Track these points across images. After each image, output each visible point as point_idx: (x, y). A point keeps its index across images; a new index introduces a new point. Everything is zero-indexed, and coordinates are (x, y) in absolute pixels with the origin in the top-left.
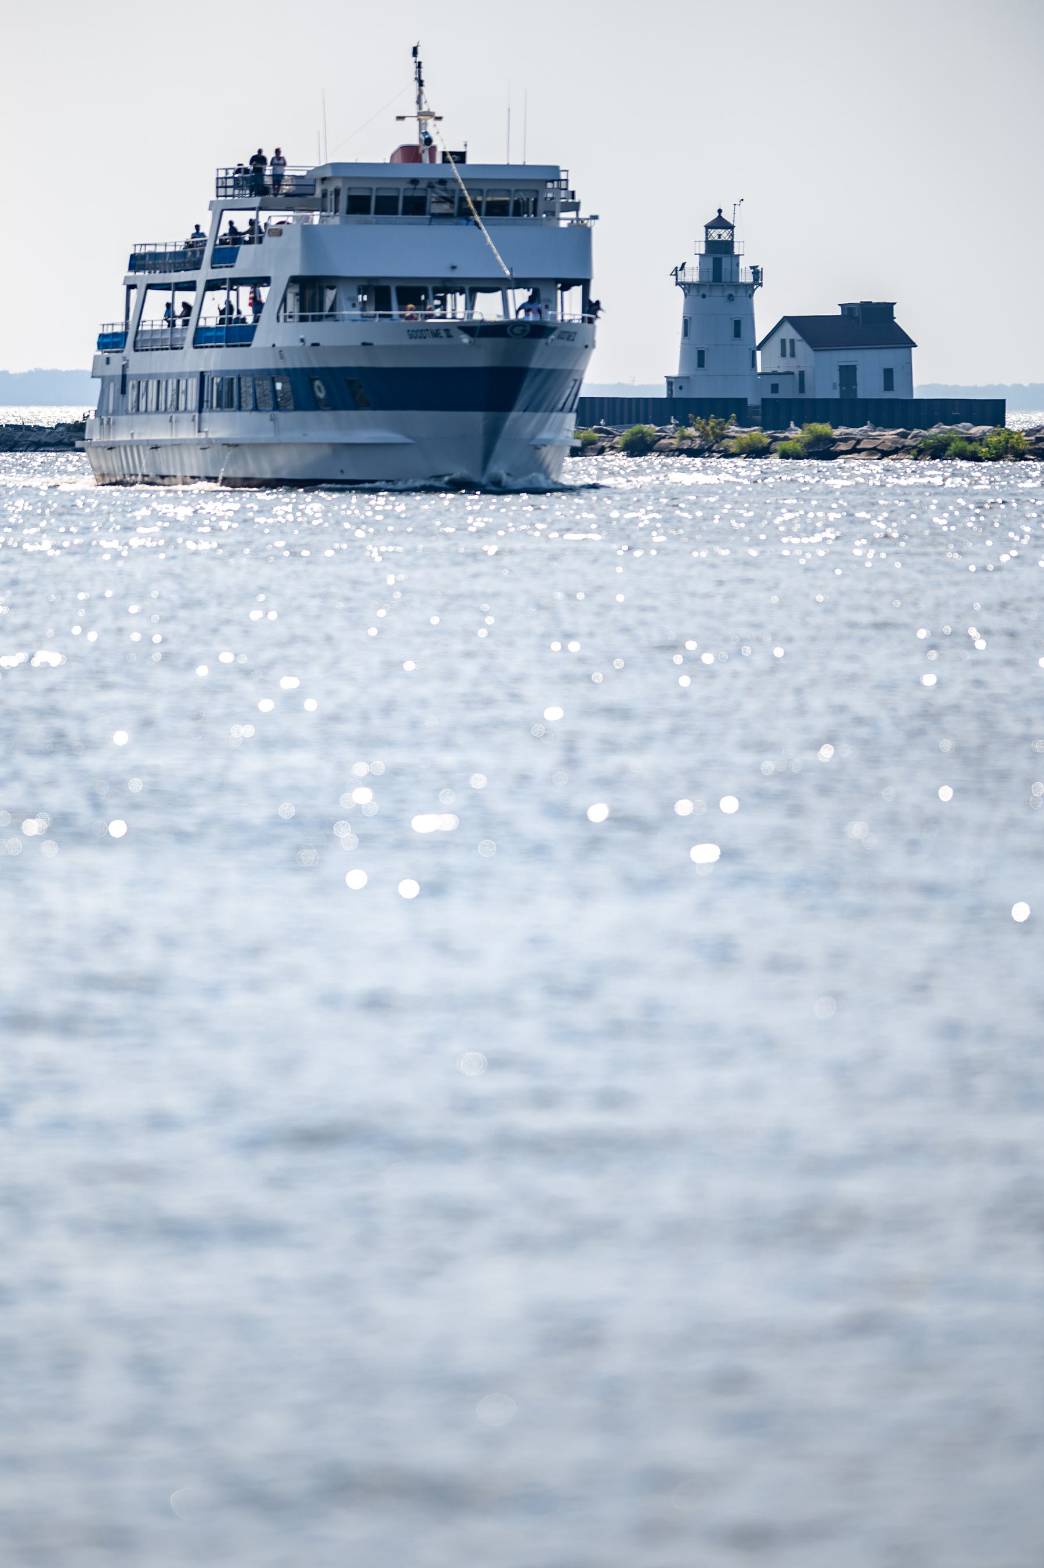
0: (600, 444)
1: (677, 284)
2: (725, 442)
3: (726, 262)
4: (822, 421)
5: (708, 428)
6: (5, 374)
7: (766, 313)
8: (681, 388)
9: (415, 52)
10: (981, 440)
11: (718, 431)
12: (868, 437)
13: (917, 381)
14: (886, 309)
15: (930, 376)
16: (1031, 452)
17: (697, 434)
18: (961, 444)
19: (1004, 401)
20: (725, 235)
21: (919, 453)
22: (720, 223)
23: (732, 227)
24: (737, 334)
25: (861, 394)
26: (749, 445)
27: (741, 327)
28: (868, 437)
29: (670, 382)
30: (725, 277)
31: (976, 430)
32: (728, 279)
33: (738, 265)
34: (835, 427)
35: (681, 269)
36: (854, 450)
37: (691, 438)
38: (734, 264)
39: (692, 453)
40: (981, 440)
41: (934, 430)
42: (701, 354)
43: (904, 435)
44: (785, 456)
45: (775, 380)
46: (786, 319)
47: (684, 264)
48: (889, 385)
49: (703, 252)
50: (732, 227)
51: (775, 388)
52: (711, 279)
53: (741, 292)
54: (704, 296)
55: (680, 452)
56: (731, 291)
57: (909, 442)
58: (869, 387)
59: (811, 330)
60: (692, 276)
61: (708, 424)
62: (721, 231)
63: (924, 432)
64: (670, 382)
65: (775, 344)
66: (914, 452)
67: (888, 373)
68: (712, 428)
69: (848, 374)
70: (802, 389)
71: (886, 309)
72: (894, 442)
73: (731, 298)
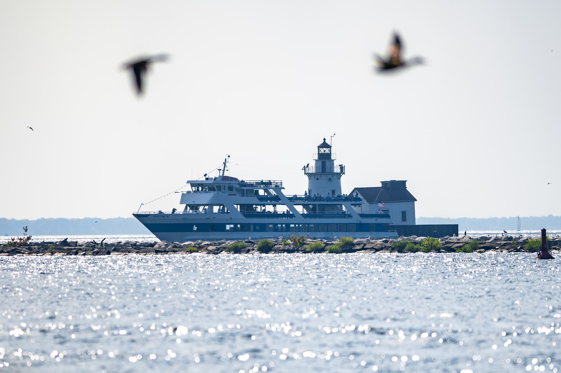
0: (248, 248)
1: (305, 174)
2: (304, 246)
6: (4, 220)
7: (347, 187)
10: (420, 243)
12: (369, 243)
13: (417, 216)
14: (403, 184)
15: (425, 213)
16: (443, 248)
17: (292, 243)
18: (412, 245)
19: (457, 225)
20: (327, 150)
21: (392, 250)
22: (325, 145)
23: (330, 147)
26: (315, 248)
28: (369, 243)
30: (327, 170)
31: (419, 239)
36: (363, 249)
37: (289, 245)
38: (332, 164)
39: (289, 251)
40: (420, 243)
43: (386, 242)
44: (331, 252)
46: (355, 189)
47: (308, 165)
48: (404, 218)
49: (317, 159)
50: (330, 147)
52: (321, 171)
53: (335, 177)
55: (284, 251)
56: (330, 176)
57: (388, 245)
58: (395, 220)
60: (312, 170)
62: (325, 149)
63: (395, 240)
66: (390, 249)
67: (404, 214)
71: (403, 184)
72: (381, 245)
73: (330, 180)
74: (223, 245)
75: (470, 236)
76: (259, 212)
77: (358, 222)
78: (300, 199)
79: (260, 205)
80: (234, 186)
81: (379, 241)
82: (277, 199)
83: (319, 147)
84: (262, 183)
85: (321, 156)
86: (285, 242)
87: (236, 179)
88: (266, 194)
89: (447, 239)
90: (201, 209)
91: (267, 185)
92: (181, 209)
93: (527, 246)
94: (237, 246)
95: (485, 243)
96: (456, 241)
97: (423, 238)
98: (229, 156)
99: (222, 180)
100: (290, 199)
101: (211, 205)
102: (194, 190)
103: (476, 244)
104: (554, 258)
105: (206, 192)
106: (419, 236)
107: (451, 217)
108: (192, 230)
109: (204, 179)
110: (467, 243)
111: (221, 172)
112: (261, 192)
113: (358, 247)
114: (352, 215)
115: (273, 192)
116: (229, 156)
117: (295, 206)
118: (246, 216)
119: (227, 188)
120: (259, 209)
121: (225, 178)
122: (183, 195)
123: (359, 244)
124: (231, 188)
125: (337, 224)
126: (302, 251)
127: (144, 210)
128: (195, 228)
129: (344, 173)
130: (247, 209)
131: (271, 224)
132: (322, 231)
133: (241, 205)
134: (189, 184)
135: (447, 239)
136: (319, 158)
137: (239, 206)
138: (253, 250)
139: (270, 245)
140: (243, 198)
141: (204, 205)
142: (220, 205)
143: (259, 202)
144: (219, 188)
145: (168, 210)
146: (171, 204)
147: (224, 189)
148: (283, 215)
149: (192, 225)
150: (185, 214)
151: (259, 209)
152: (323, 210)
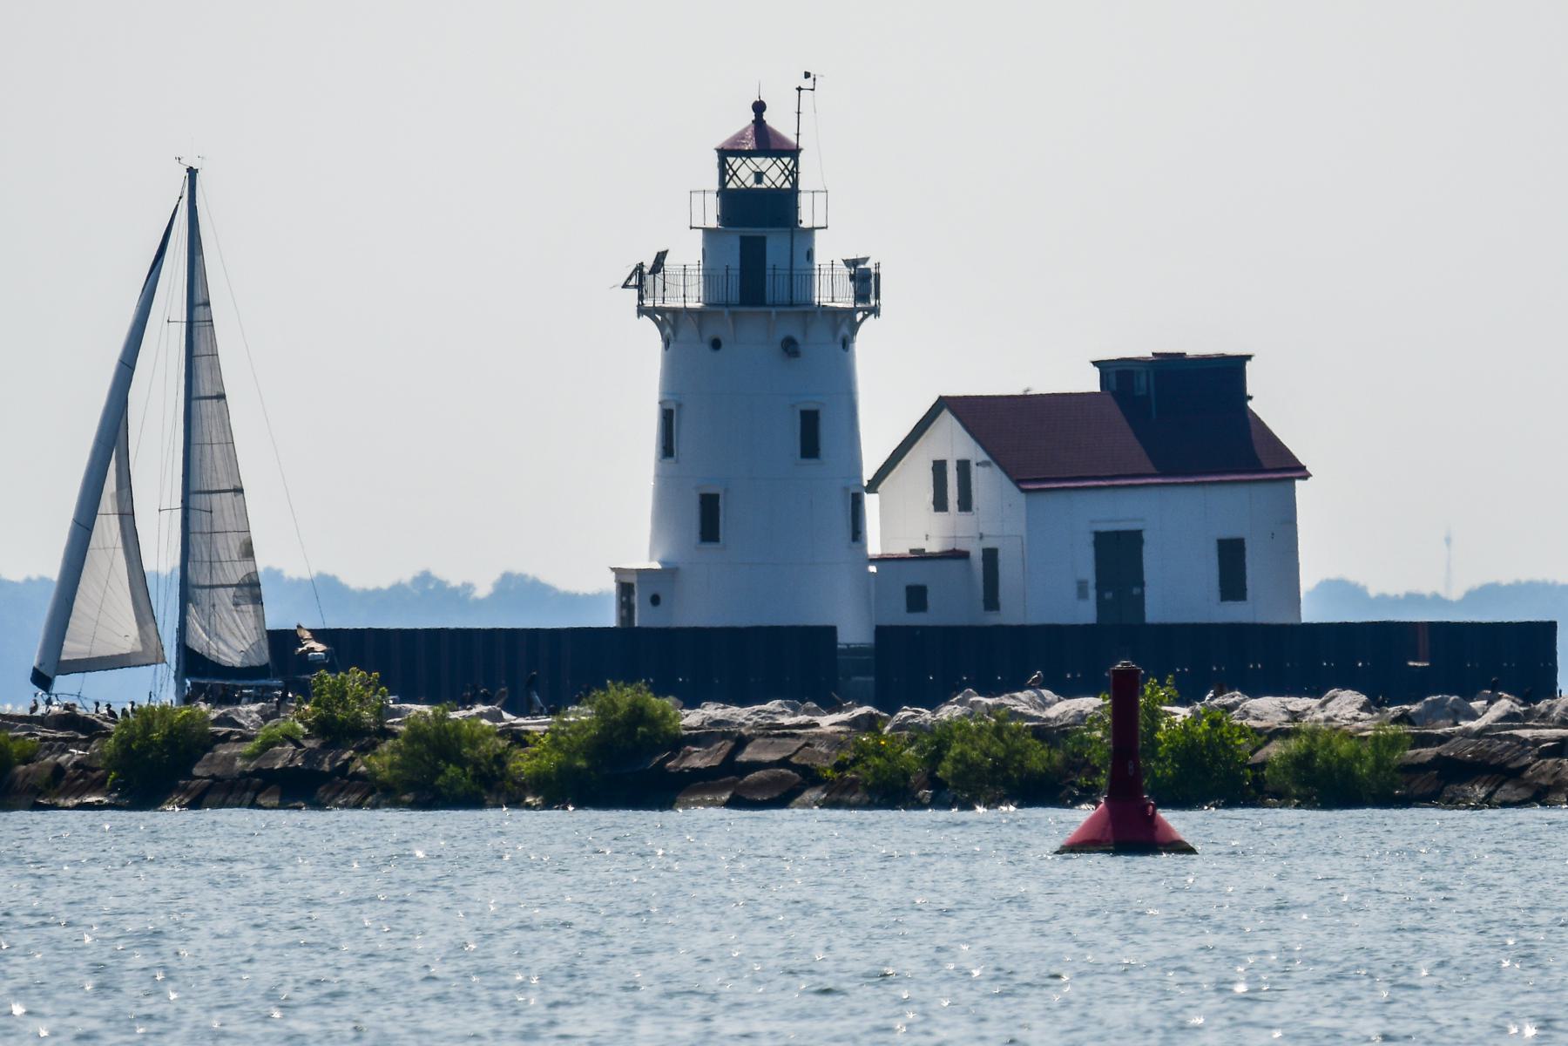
1: (642, 311)
7: (892, 384)
8: (655, 600)
14: (1227, 373)
19: (1551, 627)
22: (764, 141)
30: (775, 288)
33: (810, 255)
45: (917, 574)
46: (943, 404)
47: (661, 257)
48: (1233, 584)
49: (713, 223)
50: (794, 153)
52: (735, 296)
56: (791, 329)
62: (763, 163)
65: (917, 470)
67: (1231, 555)
69: (1119, 555)
71: (1227, 373)
73: (790, 347)
83: (724, 154)
123: (703, 737)
129: (875, 311)
136: (726, 216)
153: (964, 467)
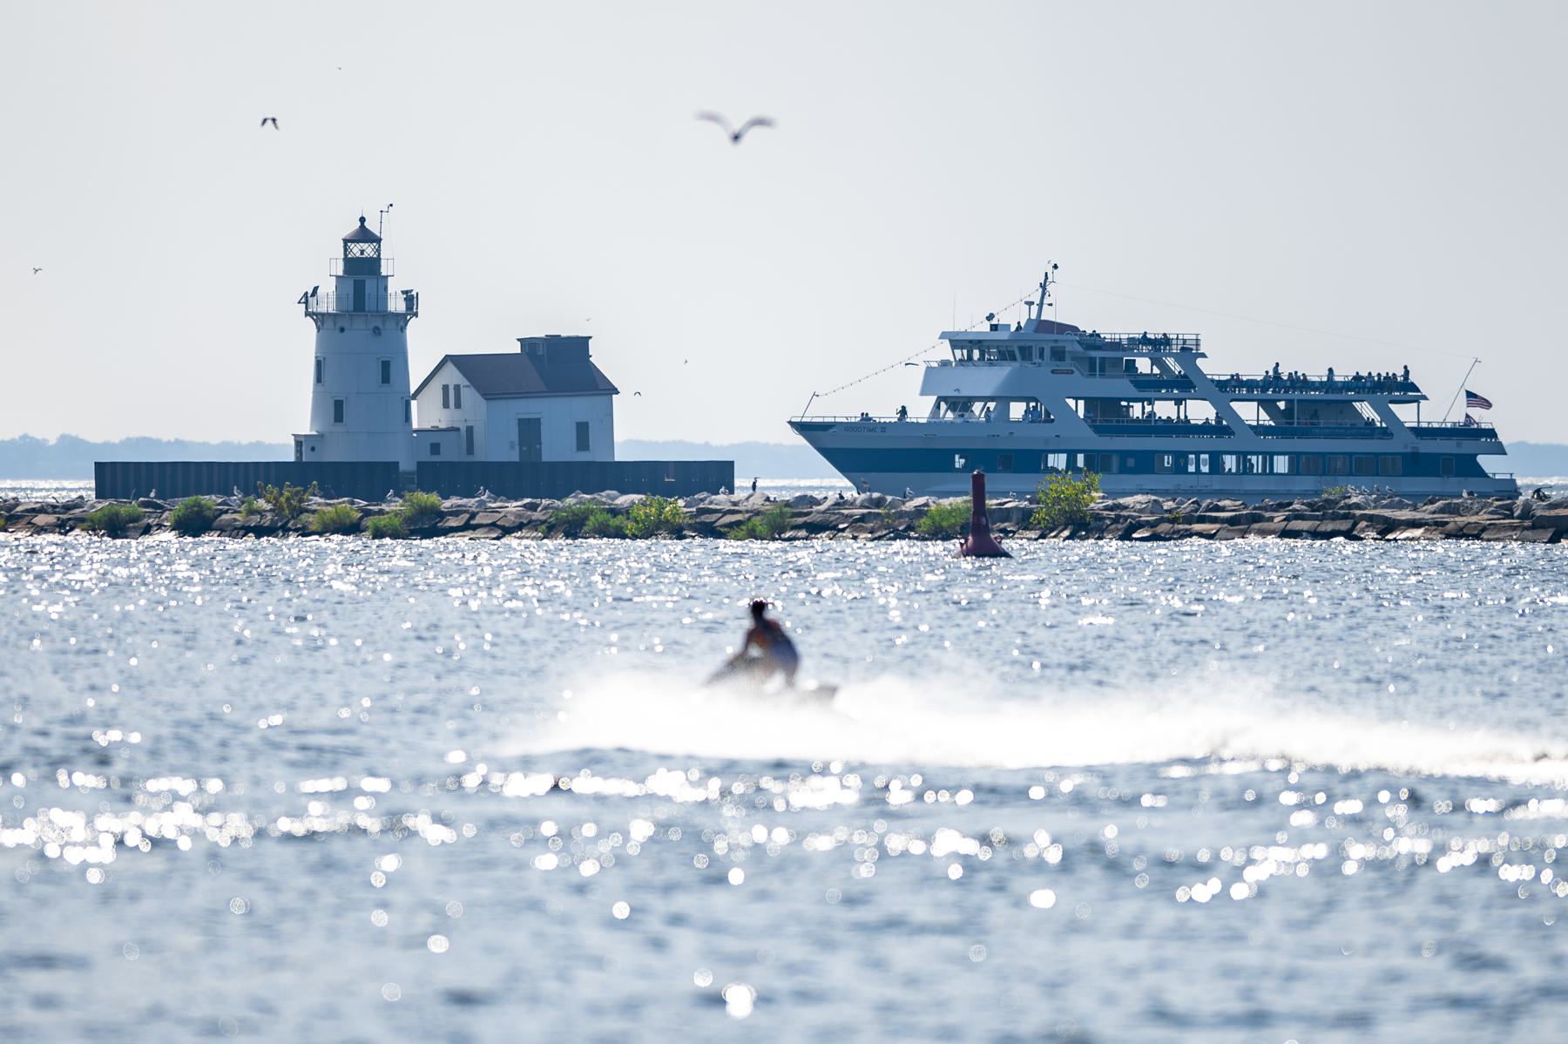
2: (304, 517)
3: (370, 286)
4: (428, 491)
5: (283, 499)
7: (423, 351)
8: (313, 449)
9: (760, 122)
11: (294, 503)
12: (486, 510)
13: (619, 436)
15: (637, 432)
16: (692, 527)
17: (269, 507)
18: (602, 517)
20: (369, 250)
21: (550, 531)
22: (364, 235)
24: (386, 378)
25: (546, 457)
27: (390, 369)
28: (486, 510)
29: (300, 442)
30: (370, 304)
31: (623, 500)
32: (373, 308)
33: (386, 289)
34: (446, 498)
35: (313, 294)
36: (467, 527)
37: (261, 512)
39: (260, 532)
41: (570, 501)
42: (339, 405)
45: (435, 439)
46: (447, 358)
47: (316, 289)
49: (341, 273)
50: (378, 240)
51: (435, 448)
53: (391, 325)
54: (342, 330)
55: (245, 530)
57: (537, 515)
58: (557, 447)
59: (477, 371)
60: (327, 304)
61: (281, 494)
62: (364, 246)
63: (558, 503)
64: (300, 442)
67: (582, 430)
68: (288, 499)
69: (529, 430)
70: (470, 450)
72: (518, 515)
74: (77, 511)
75: (767, 493)
76: (1133, 421)
77: (1409, 450)
78: (1251, 385)
79: (1141, 400)
80: (1069, 348)
81: (513, 506)
82: (1186, 385)
83: (346, 241)
84: (1145, 340)
85: (352, 265)
86: (250, 504)
87: (1075, 329)
88: (1156, 371)
89: (702, 500)
90: (977, 407)
91: (1157, 346)
92: (921, 410)
93: (924, 522)
94: (117, 514)
95: (807, 514)
96: (728, 507)
97: (636, 497)
98: (1056, 267)
99: (1036, 331)
100: (1222, 385)
101: (1004, 400)
102: (959, 356)
103: (782, 514)
104: (1007, 555)
105: (991, 363)
106: (623, 492)
107: (716, 441)
108: (950, 467)
109: (986, 327)
110: (757, 513)
111: (1035, 308)
112: (1144, 365)
113: (453, 522)
114: (1392, 429)
115: (1176, 368)
116: (1056, 267)
117: (1234, 405)
118: (1099, 430)
119: (1047, 353)
120: (1137, 411)
121: (1043, 326)
122: (929, 369)
123: (455, 513)
124: (1058, 354)
125: (1351, 454)
126: (296, 530)
127: (820, 412)
128: (959, 462)
129: (416, 315)
130: (1106, 413)
131: (1168, 453)
132: (1309, 473)
133: (1090, 402)
134: (947, 343)
135: (702, 500)
137: (1081, 403)
138: (160, 526)
139: (208, 513)
140: (1092, 380)
141: (986, 399)
142: (1027, 400)
143: (1135, 393)
144: (1026, 353)
145: (887, 414)
146: (897, 394)
147: (1041, 356)
148: (1205, 429)
149: (948, 455)
150: (934, 423)
151: (1137, 411)
152: (1315, 415)
153: (457, 388)
